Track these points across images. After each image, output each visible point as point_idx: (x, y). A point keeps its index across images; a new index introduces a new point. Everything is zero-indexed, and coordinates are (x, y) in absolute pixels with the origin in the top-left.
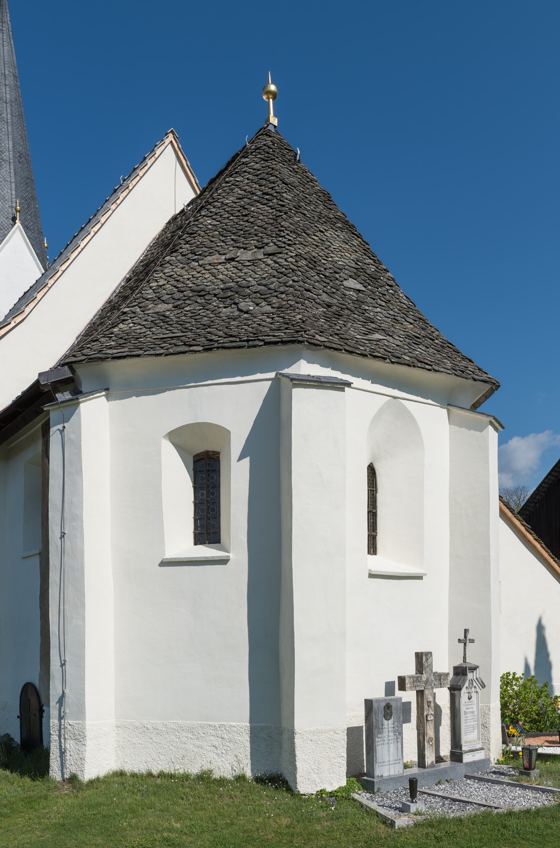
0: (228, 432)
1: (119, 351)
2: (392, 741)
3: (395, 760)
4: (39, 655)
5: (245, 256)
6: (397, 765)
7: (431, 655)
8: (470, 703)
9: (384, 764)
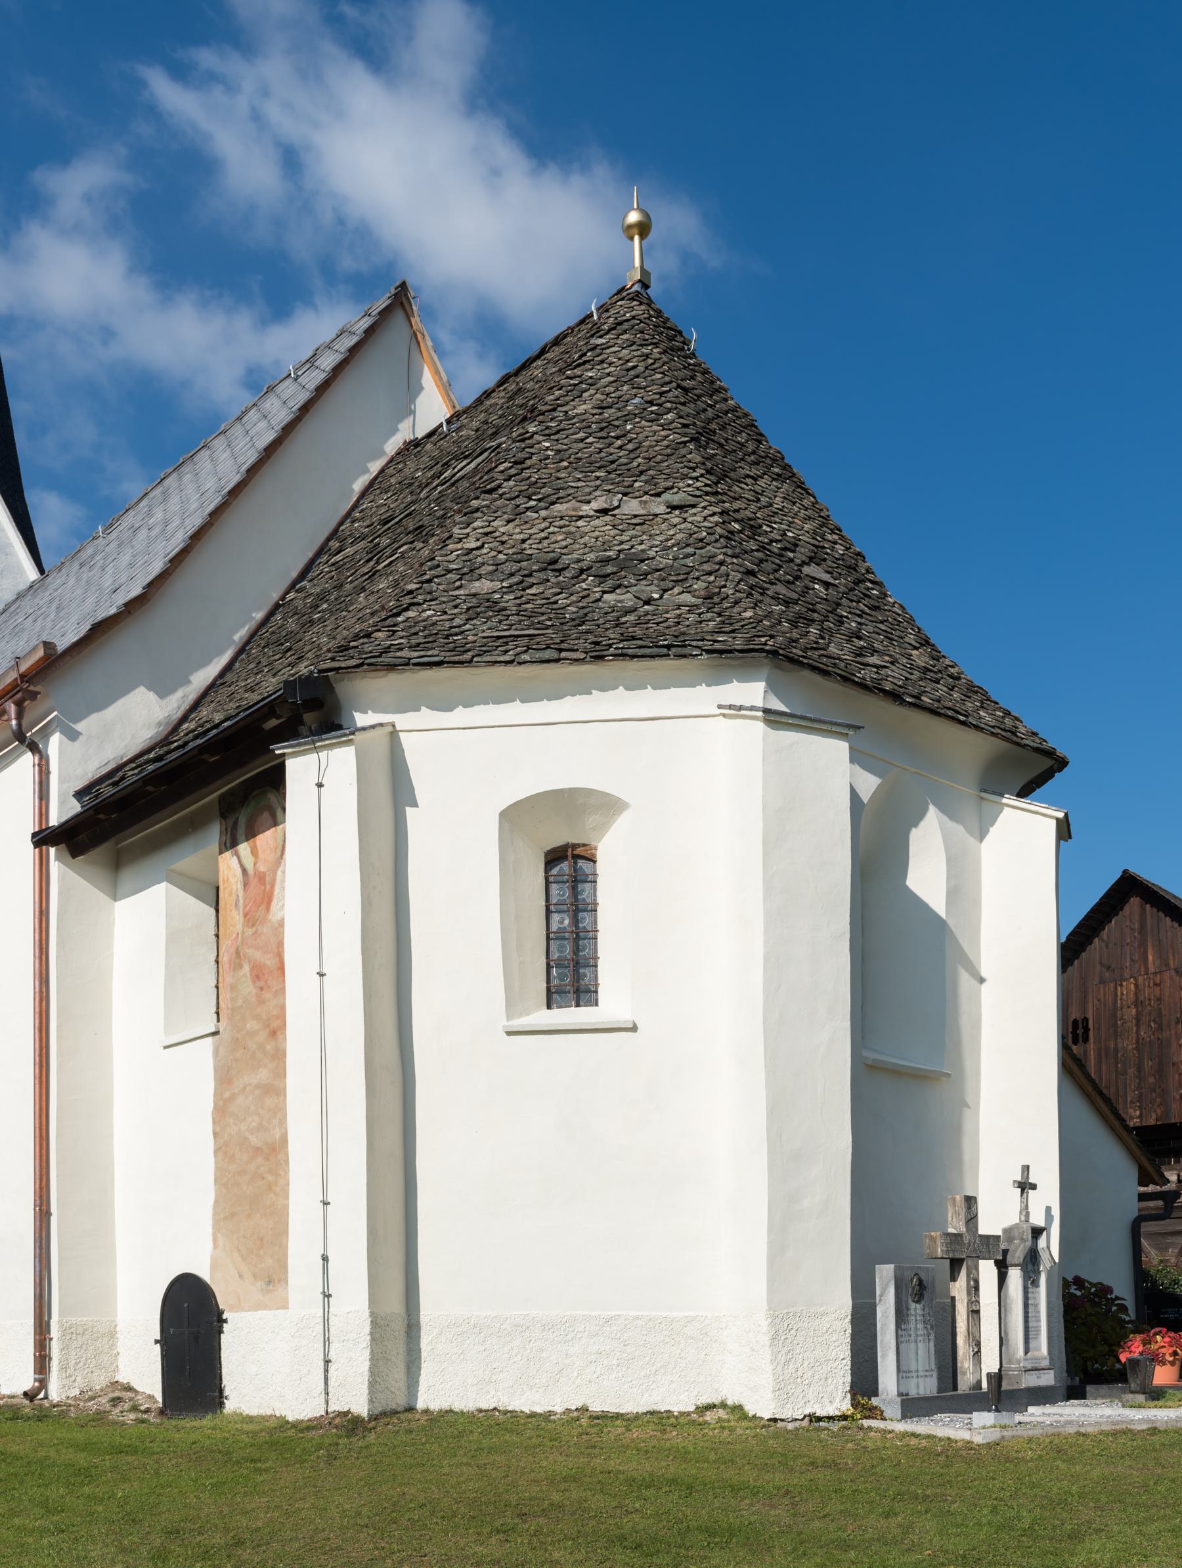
1: (422, 653)
4: (210, 1222)
5: (632, 506)
6: (928, 1379)
7: (976, 1202)
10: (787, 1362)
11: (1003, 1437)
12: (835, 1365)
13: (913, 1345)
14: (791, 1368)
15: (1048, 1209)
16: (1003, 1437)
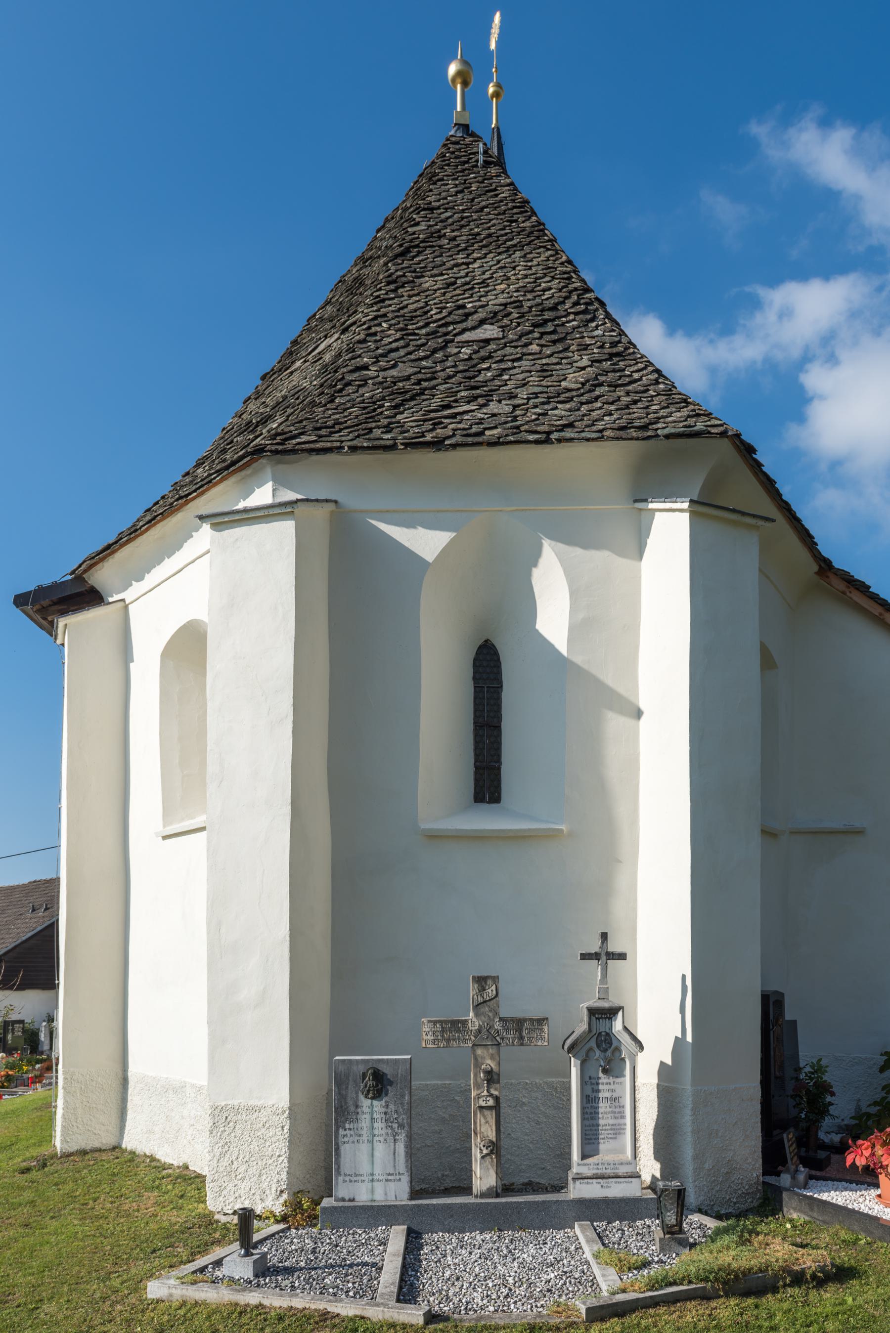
2: (382, 1139)
3: (389, 1174)
9: (360, 1178)
10: (222, 1155)
11: (171, 1295)
12: (271, 1161)
13: (364, 1148)
14: (225, 1162)
15: (684, 977)
16: (171, 1295)
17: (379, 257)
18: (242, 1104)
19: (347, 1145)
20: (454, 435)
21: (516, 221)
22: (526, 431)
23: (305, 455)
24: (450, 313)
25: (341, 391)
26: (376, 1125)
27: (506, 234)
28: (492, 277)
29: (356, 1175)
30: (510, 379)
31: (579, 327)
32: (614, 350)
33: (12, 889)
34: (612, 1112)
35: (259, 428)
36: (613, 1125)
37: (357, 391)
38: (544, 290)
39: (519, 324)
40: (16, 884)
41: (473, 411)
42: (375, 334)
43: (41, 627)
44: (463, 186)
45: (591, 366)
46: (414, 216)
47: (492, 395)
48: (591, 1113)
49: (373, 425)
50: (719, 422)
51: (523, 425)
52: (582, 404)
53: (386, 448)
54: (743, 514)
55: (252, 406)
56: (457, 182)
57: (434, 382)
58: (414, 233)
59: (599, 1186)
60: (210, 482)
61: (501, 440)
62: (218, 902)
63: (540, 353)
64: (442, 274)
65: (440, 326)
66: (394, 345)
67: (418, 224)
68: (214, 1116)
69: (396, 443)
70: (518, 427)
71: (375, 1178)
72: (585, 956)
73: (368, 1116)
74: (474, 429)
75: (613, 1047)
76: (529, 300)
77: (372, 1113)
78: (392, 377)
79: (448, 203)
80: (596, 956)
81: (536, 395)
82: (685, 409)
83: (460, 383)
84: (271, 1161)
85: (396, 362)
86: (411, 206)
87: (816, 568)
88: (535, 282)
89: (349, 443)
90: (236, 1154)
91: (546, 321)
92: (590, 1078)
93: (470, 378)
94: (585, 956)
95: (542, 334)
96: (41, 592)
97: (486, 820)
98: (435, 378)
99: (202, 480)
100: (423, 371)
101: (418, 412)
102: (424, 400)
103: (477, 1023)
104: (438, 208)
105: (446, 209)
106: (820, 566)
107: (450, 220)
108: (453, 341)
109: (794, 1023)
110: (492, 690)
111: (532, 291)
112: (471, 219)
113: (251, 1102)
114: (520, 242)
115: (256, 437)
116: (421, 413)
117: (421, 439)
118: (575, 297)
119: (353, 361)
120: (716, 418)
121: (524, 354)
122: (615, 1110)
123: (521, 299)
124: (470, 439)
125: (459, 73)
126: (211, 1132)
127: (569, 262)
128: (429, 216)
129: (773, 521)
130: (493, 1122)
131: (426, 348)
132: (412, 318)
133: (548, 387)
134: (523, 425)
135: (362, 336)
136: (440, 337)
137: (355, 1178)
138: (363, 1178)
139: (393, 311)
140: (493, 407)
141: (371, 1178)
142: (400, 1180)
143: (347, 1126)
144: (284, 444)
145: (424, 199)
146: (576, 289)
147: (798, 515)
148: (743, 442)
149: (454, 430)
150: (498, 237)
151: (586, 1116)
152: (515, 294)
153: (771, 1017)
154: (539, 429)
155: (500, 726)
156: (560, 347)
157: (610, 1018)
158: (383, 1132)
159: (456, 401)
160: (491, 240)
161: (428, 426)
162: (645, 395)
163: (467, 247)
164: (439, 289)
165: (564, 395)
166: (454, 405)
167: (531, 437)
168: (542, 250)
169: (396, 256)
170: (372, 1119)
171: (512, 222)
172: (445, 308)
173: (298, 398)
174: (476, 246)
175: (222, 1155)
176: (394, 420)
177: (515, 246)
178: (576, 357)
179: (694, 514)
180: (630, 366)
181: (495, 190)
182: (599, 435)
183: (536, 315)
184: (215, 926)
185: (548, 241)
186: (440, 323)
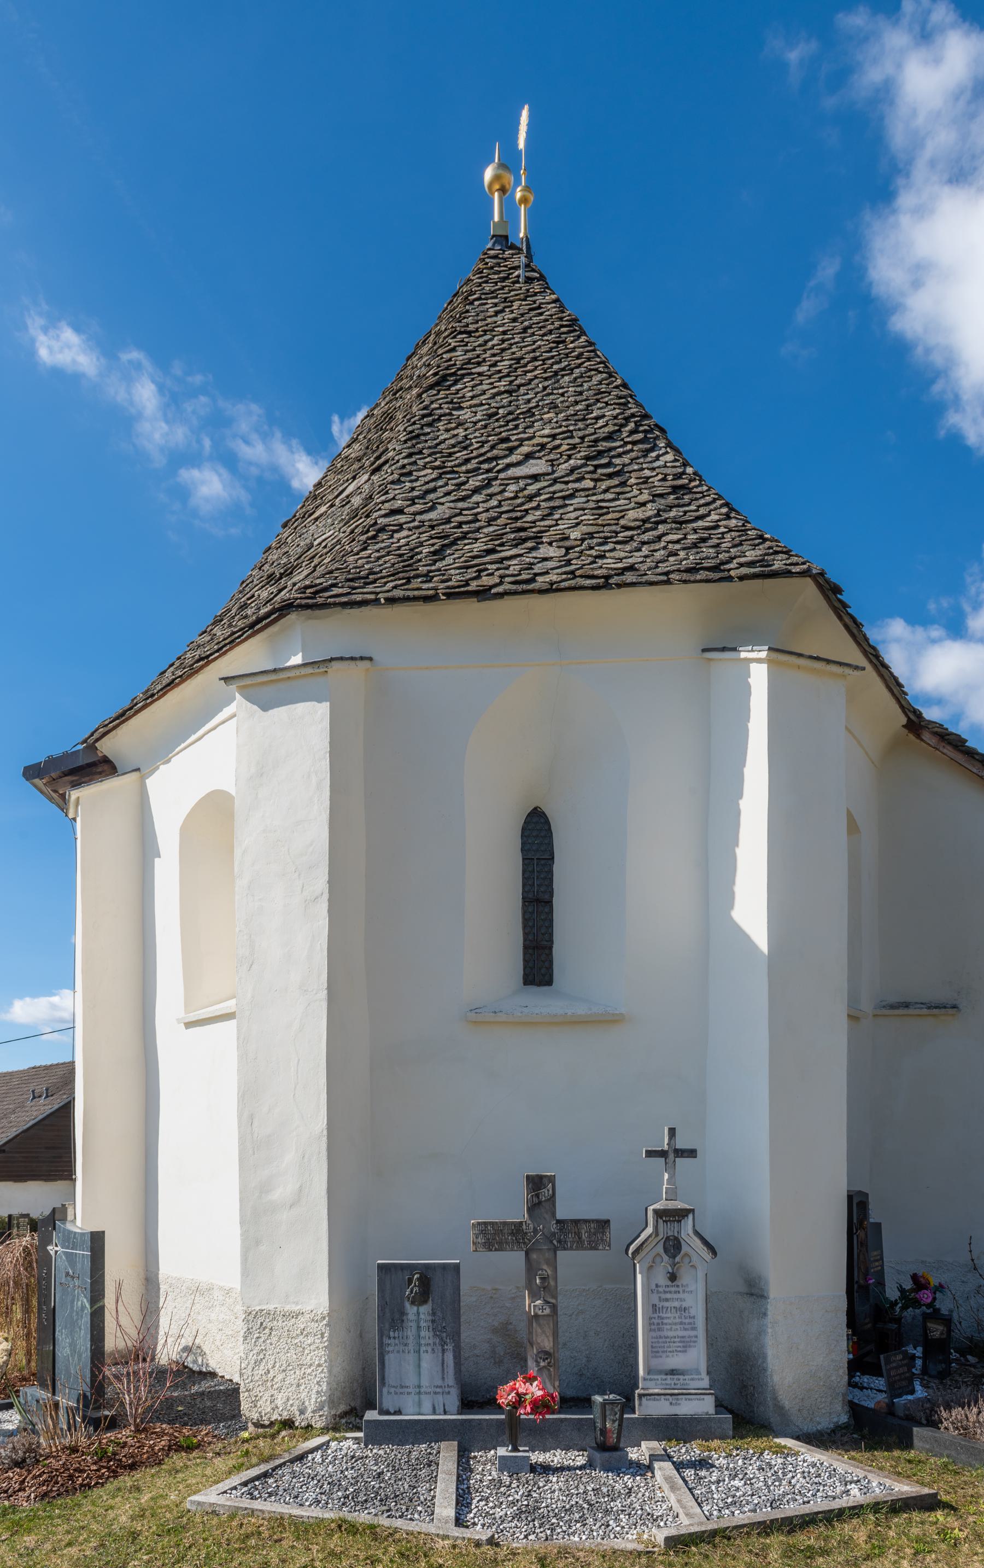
0: (265, 708)
2: (429, 1349)
3: (437, 1387)
8: (673, 1289)
9: (406, 1390)
10: (257, 1363)
12: (309, 1371)
13: (411, 1358)
14: (261, 1370)
17: (410, 387)
18: (278, 1310)
19: (391, 1355)
20: (501, 583)
21: (564, 342)
22: (581, 576)
23: (339, 609)
24: (493, 447)
25: (374, 537)
26: (422, 1334)
27: (553, 357)
28: (538, 406)
29: (402, 1387)
30: (561, 519)
31: (638, 458)
32: (680, 482)
33: (11, 1074)
34: (681, 1323)
35: (283, 581)
36: (683, 1337)
37: (392, 537)
38: (597, 418)
39: (570, 457)
40: (15, 1069)
41: (521, 555)
42: (410, 473)
43: (51, 799)
44: (503, 305)
45: (653, 501)
46: (450, 341)
47: (541, 537)
48: (658, 1324)
49: (412, 574)
50: (801, 560)
51: (578, 569)
52: (644, 543)
53: (426, 599)
54: (828, 661)
55: (273, 556)
56: (496, 301)
57: (477, 525)
58: (450, 360)
59: (668, 1403)
60: (233, 641)
61: (554, 587)
62: (249, 1095)
63: (594, 488)
64: (482, 404)
65: (481, 463)
66: (432, 485)
67: (454, 350)
68: (248, 1321)
69: (437, 594)
70: (572, 572)
71: (422, 1390)
72: (650, 1154)
73: (414, 1325)
74: (524, 576)
75: (682, 1252)
76: (579, 430)
77: (418, 1321)
78: (430, 520)
79: (487, 325)
80: (663, 1154)
81: (591, 535)
82: (761, 547)
83: (506, 525)
84: (309, 1371)
85: (434, 504)
86: (446, 329)
87: (904, 720)
88: (586, 409)
89: (386, 595)
90: (272, 1362)
91: (600, 454)
92: (657, 1286)
93: (517, 519)
94: (650, 1154)
95: (596, 467)
96: (52, 762)
97: (539, 1002)
98: (478, 521)
99: (224, 639)
100: (464, 512)
101: (459, 558)
102: (465, 545)
103: (531, 1226)
104: (477, 330)
105: (485, 331)
106: (909, 718)
107: (490, 344)
108: (496, 478)
109: (878, 1226)
110: (543, 862)
111: (584, 419)
112: (513, 341)
113: (288, 1308)
114: (569, 365)
115: (280, 591)
116: (462, 559)
117: (466, 589)
118: (631, 426)
119: (386, 505)
120: (796, 556)
121: (577, 490)
122: (684, 1321)
123: (571, 428)
124: (520, 588)
125: (496, 178)
126: (245, 1338)
127: (625, 385)
128: (466, 340)
129: (863, 669)
130: (549, 1332)
131: (466, 487)
132: (450, 455)
133: (604, 526)
134: (578, 569)
135: (396, 476)
136: (483, 474)
137: (402, 1390)
138: (409, 1390)
139: (430, 447)
140: (545, 551)
141: (417, 1390)
142: (449, 1393)
143: (392, 1334)
144: (315, 598)
145: (460, 322)
146: (633, 415)
147: (886, 661)
148: (827, 581)
149: (502, 577)
150: (544, 360)
151: (653, 1327)
152: (564, 423)
153: (855, 1221)
154: (596, 573)
155: (551, 902)
156: (615, 481)
157: (679, 1221)
158: (431, 1342)
159: (502, 545)
160: (537, 363)
161: (471, 573)
162: (716, 532)
163: (510, 372)
164: (480, 421)
165: (622, 534)
166: (499, 549)
167: (588, 582)
168: (593, 373)
169: (431, 387)
170: (419, 1327)
171: (558, 343)
172: (487, 442)
173: (325, 547)
174: (519, 372)
175: (257, 1363)
176: (433, 568)
177: (563, 369)
178: (636, 492)
179: (769, 661)
180: (696, 499)
181: (539, 308)
182: (665, 578)
183: (589, 446)
184: (247, 1119)
185: (600, 363)
186: (481, 459)
